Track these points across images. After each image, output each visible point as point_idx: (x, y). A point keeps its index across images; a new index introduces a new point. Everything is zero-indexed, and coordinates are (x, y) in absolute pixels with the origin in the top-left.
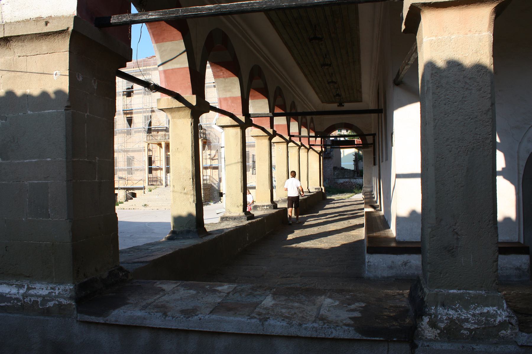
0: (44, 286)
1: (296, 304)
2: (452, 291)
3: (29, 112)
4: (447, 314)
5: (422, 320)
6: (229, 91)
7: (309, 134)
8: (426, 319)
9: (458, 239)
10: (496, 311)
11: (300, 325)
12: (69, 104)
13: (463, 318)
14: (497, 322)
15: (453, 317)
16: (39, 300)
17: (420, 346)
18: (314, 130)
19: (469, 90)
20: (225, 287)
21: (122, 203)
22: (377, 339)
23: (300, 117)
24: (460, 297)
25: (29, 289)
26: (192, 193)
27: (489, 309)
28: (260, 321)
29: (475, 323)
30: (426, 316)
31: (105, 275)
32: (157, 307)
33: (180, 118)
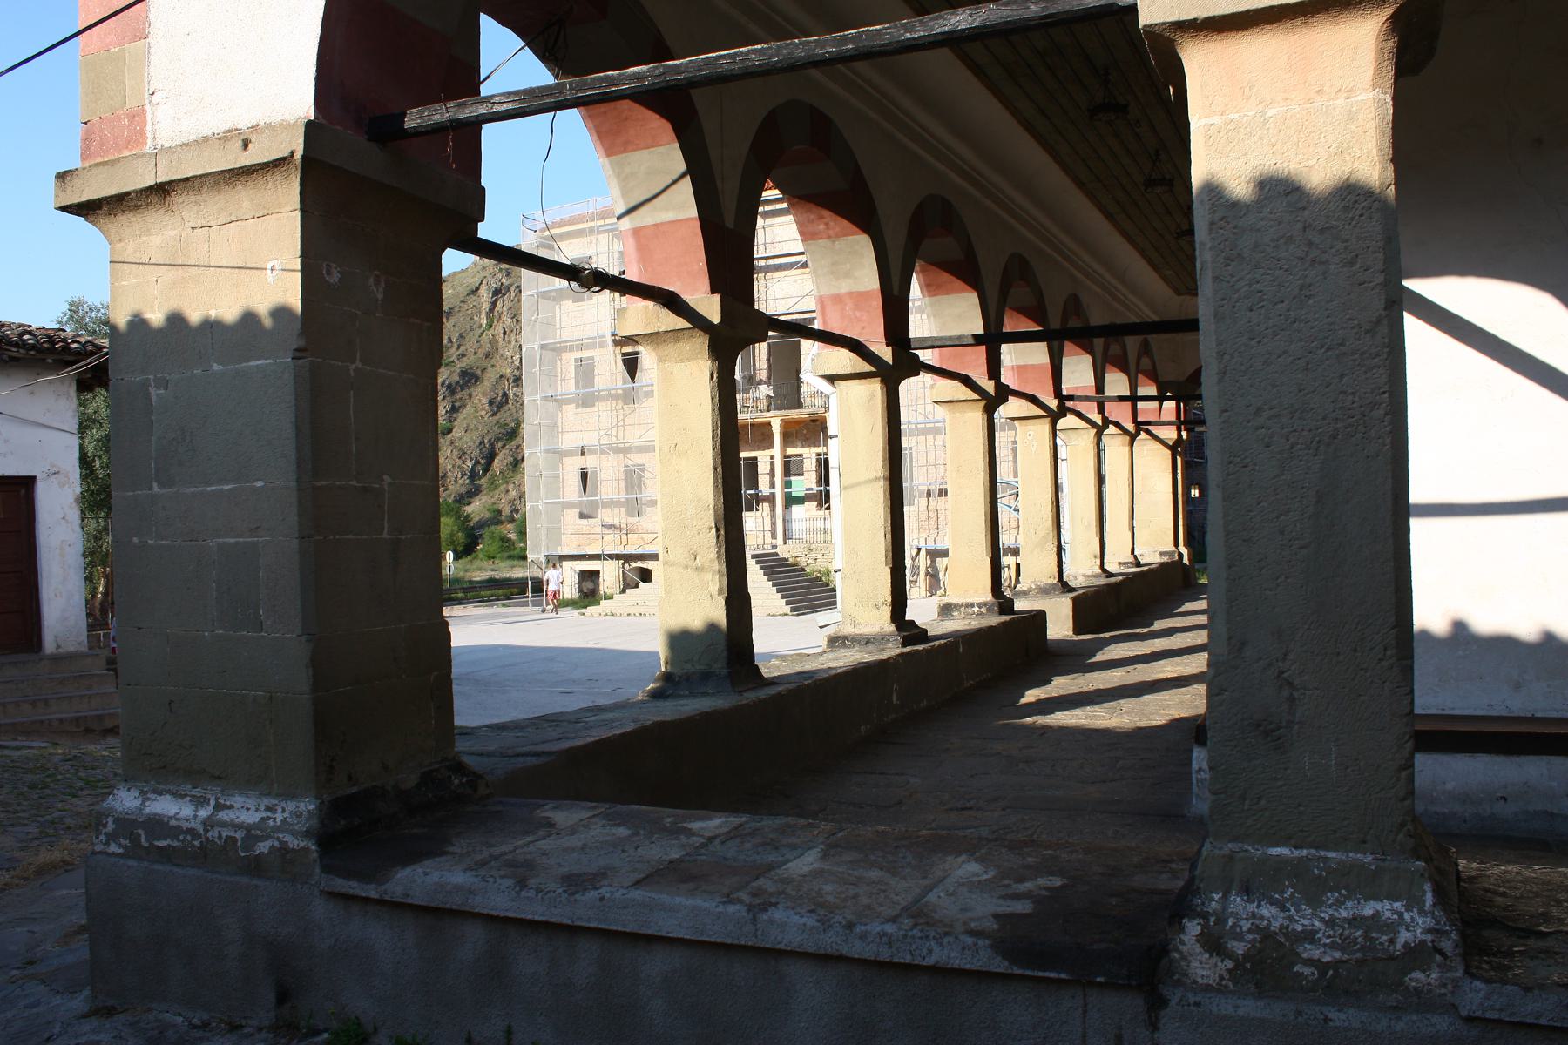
0: (250, 803)
1: (874, 874)
2: (1275, 851)
3: (216, 367)
4: (1254, 915)
5: (1182, 930)
6: (847, 275)
7: (1133, 387)
8: (1193, 928)
9: (1292, 699)
10: (1401, 915)
11: (850, 926)
12: (302, 343)
13: (1300, 928)
14: (1398, 947)
15: (1269, 923)
16: (239, 835)
17: (1173, 1003)
18: (1153, 377)
19: (1321, 263)
20: (715, 823)
21: (609, 597)
22: (1053, 975)
23: (1098, 342)
24: (1297, 870)
25: (219, 807)
26: (716, 566)
27: (1378, 906)
28: (749, 911)
29: (1333, 946)
30: (1192, 918)
31: (410, 780)
32: (512, 864)
33: (681, 361)
